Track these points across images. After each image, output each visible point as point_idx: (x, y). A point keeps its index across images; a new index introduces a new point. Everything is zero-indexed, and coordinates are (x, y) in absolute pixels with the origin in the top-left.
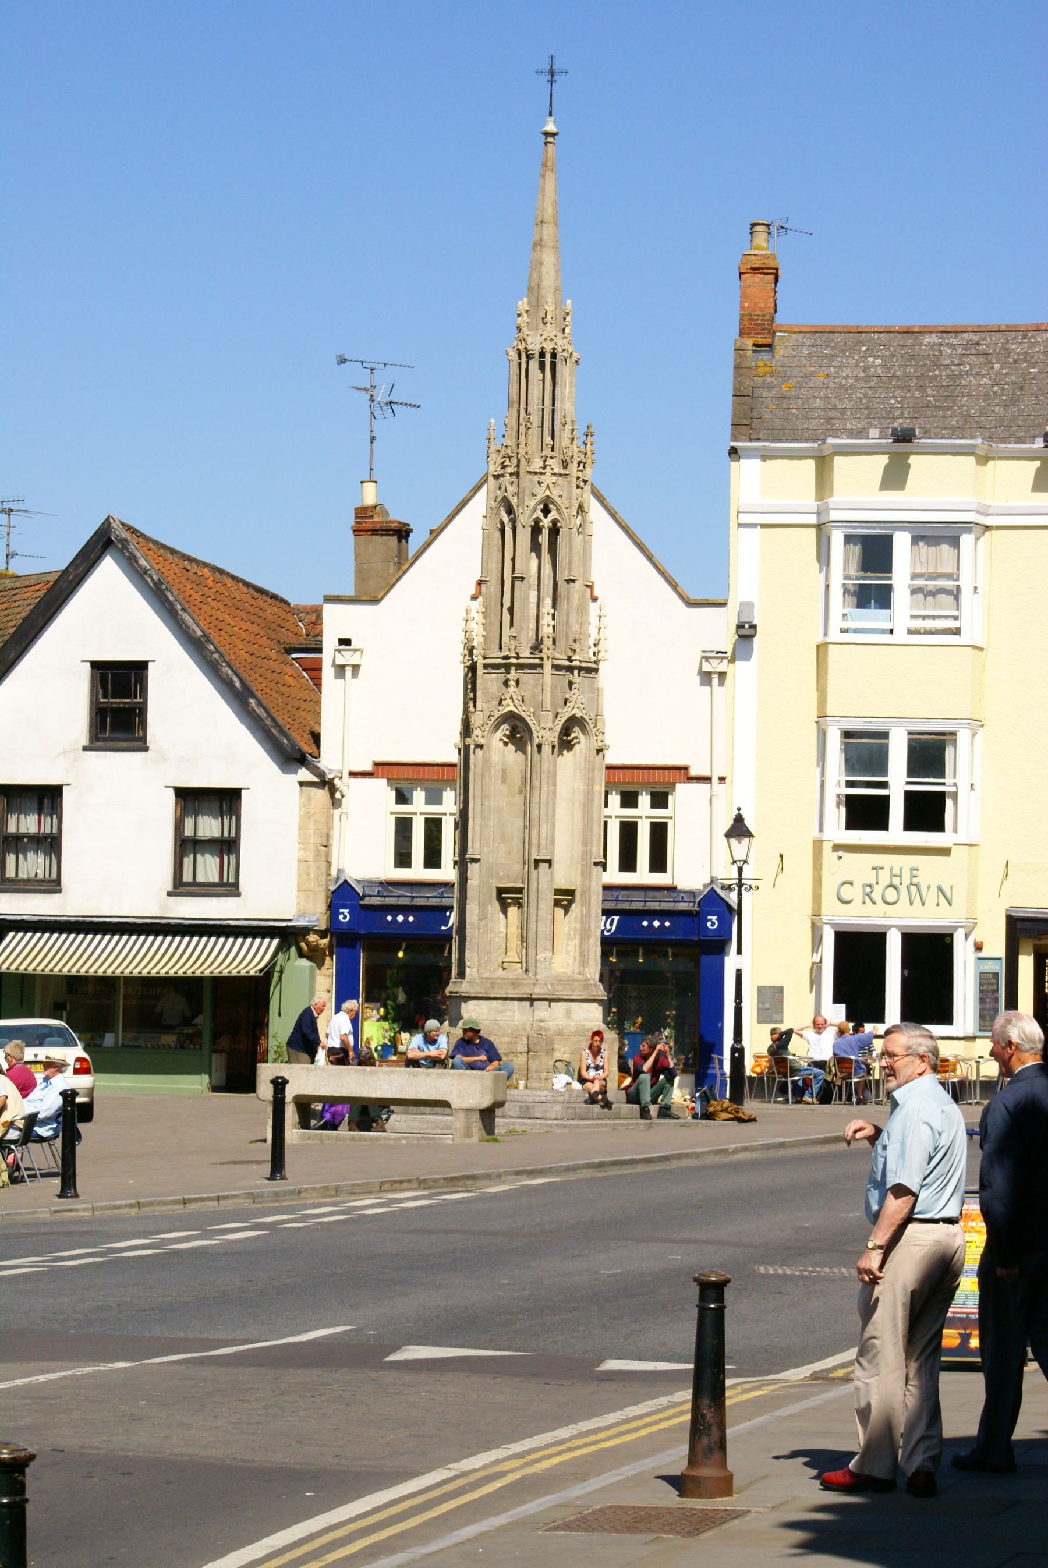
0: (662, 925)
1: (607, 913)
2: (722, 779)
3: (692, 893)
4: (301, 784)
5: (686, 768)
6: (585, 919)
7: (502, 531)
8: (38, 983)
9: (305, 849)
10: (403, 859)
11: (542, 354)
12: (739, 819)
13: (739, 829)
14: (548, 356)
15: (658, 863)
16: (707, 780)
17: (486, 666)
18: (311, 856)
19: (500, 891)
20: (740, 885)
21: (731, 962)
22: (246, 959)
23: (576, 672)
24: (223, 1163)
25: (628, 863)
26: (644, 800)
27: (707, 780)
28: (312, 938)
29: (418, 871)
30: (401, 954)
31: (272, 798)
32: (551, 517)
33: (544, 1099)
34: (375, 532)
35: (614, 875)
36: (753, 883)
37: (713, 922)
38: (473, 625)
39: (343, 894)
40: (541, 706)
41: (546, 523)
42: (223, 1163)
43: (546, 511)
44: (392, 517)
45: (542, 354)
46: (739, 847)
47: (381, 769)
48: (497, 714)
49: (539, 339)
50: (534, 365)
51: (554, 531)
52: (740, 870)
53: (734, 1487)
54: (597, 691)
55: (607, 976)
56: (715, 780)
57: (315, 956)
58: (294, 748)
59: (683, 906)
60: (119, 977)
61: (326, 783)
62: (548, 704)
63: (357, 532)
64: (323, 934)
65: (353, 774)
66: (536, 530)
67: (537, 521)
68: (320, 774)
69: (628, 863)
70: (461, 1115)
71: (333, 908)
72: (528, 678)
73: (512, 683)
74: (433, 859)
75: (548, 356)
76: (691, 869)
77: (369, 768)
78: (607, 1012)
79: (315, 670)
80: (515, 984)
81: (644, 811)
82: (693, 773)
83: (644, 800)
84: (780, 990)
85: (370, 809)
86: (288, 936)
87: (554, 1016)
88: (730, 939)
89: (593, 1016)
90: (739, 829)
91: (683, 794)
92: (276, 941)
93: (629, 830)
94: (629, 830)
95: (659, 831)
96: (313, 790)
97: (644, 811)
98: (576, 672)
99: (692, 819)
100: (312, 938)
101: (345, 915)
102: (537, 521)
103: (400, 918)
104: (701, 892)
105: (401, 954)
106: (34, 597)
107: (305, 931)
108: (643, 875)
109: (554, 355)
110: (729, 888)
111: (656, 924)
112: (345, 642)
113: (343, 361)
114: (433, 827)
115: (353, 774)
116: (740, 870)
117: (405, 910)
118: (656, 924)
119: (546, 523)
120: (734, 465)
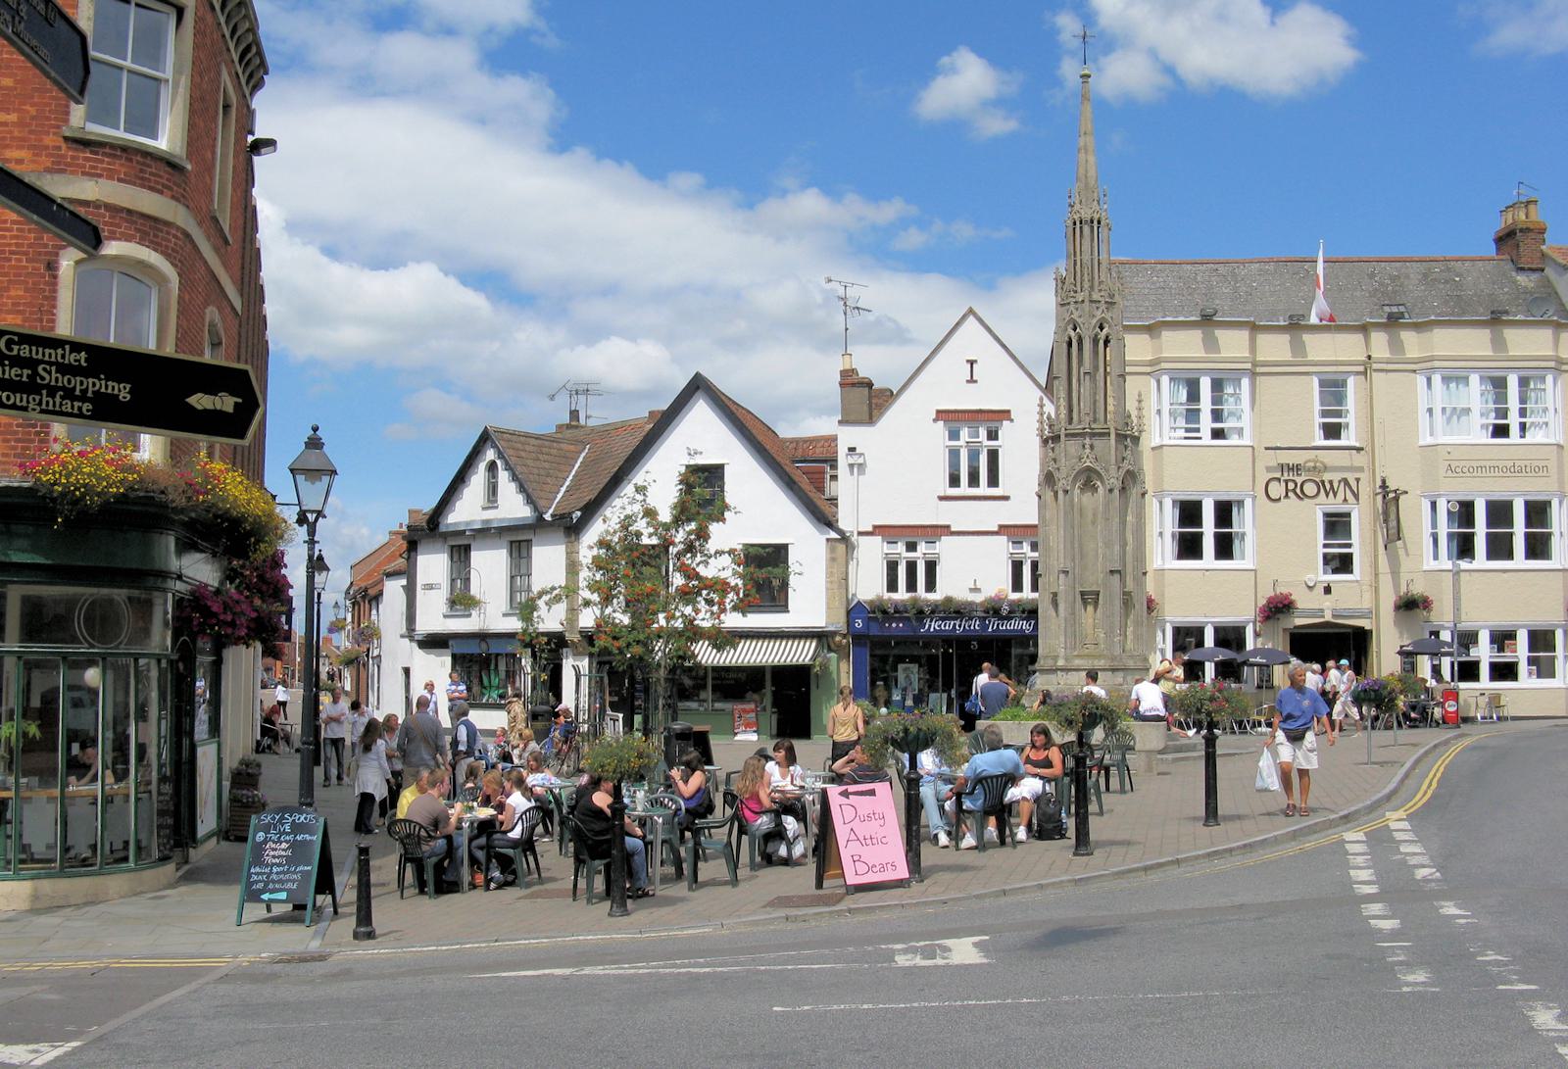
0: (890, 625)
4: (828, 540)
5: (948, 527)
7: (1070, 344)
8: (768, 677)
9: (831, 582)
10: (892, 586)
14: (1095, 222)
15: (931, 586)
17: (1066, 435)
18: (836, 586)
19: (1082, 594)
22: (800, 653)
24: (1239, 817)
31: (807, 547)
34: (853, 385)
39: (854, 610)
41: (1102, 335)
42: (1239, 817)
43: (1101, 328)
44: (861, 375)
45: (1092, 222)
47: (878, 530)
48: (1077, 469)
49: (1090, 212)
50: (1086, 229)
57: (843, 653)
58: (823, 516)
60: (764, 667)
61: (844, 538)
62: (1113, 461)
63: (841, 385)
64: (844, 636)
65: (860, 534)
66: (1095, 341)
67: (1096, 336)
68: (841, 532)
69: (912, 586)
71: (849, 623)
72: (1098, 443)
73: (1087, 446)
75: (1095, 222)
77: (870, 529)
82: (953, 529)
86: (821, 636)
96: (838, 544)
100: (838, 638)
101: (859, 624)
106: (639, 437)
107: (834, 634)
109: (1099, 222)
112: (852, 450)
114: (912, 567)
115: (860, 534)
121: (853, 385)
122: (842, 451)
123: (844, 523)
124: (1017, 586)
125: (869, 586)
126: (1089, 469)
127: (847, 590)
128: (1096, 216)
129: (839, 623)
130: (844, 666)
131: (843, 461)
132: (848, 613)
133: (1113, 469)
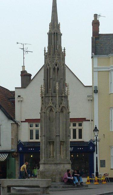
0: (82, 149)
1: (71, 147)
2: (92, 120)
3: (87, 143)
5: (85, 118)
6: (66, 148)
11: (54, 33)
12: (96, 128)
13: (96, 130)
15: (80, 137)
16: (89, 120)
20: (96, 140)
21: (95, 155)
23: (63, 97)
25: (75, 137)
26: (77, 125)
27: (89, 120)
28: (15, 154)
29: (34, 140)
30: (32, 156)
32: (57, 66)
33: (59, 184)
34: (25, 75)
35: (72, 139)
36: (99, 140)
37: (91, 148)
38: (43, 89)
39: (20, 144)
40: (56, 105)
41: (56, 67)
43: (56, 65)
45: (54, 33)
46: (96, 133)
47: (27, 121)
51: (58, 69)
52: (96, 137)
53: (7, 174)
54: (68, 101)
55: (71, 159)
56: (91, 120)
59: (85, 145)
66: (54, 69)
67: (54, 67)
68: (15, 122)
69: (75, 137)
70: (42, 189)
71: (18, 148)
74: (37, 138)
76: (86, 138)
77: (24, 120)
78: (72, 166)
79: (14, 102)
80: (53, 161)
81: (77, 127)
83: (77, 125)
84: (105, 160)
85: (25, 129)
86: (9, 153)
87: (61, 167)
88: (95, 151)
89: (69, 167)
90: (96, 130)
91: (84, 123)
92: (8, 154)
93: (74, 131)
94: (74, 131)
95: (80, 131)
97: (77, 127)
98: (63, 97)
99: (86, 128)
100: (15, 154)
101: (21, 149)
102: (54, 67)
103: (31, 149)
104: (89, 142)
105: (32, 156)
107: (13, 152)
108: (77, 139)
109: (57, 34)
110: (94, 141)
111: (80, 149)
112: (19, 96)
113: (18, 43)
116: (96, 137)
117: (32, 148)
118: (80, 149)
119: (56, 67)
120: (96, 84)
121: (25, 75)
122: (16, 97)
123: (17, 119)
124: (31, 138)
125: (25, 137)
126: (51, 106)
127: (17, 139)
128: (56, 32)
129: (15, 149)
130: (17, 162)
131: (17, 99)
132: (18, 146)
133: (58, 106)
